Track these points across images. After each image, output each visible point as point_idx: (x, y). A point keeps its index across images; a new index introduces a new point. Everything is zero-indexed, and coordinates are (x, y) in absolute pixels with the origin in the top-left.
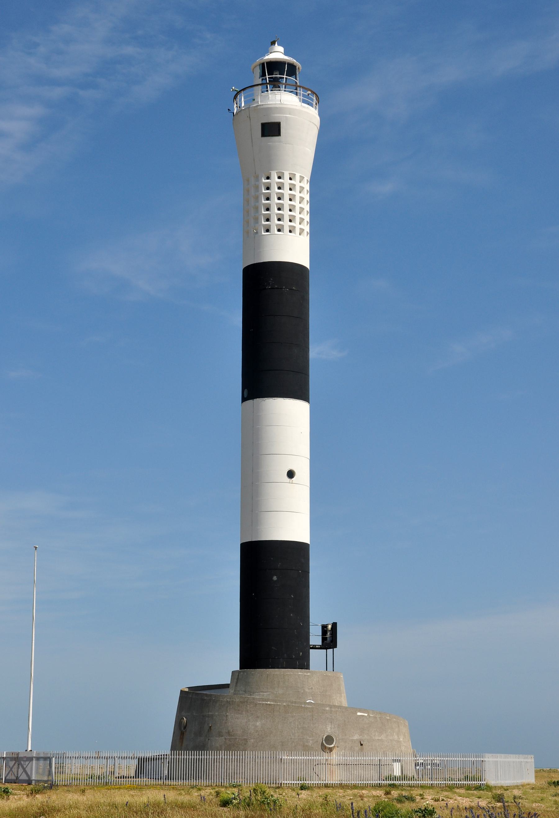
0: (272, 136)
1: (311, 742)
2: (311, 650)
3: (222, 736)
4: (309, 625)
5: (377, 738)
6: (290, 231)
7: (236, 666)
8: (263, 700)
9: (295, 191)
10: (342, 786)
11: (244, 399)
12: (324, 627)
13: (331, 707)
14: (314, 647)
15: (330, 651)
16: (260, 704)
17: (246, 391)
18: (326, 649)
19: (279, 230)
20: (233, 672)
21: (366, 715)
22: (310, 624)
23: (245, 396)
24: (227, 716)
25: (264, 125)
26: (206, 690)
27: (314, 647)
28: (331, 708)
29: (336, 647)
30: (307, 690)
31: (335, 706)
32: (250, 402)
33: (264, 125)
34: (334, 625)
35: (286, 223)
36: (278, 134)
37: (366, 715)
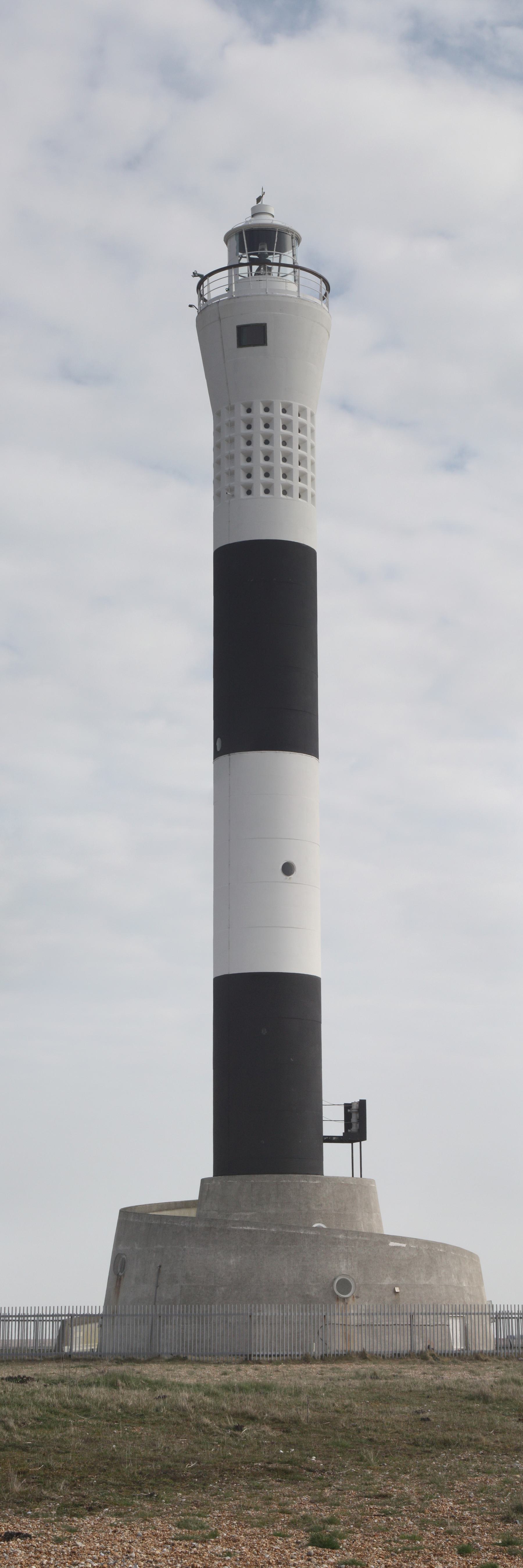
0: (254, 345)
1: (315, 1289)
2: (326, 1146)
3: (177, 1282)
4: (321, 1105)
5: (422, 1282)
6: (285, 493)
7: (208, 1172)
8: (243, 1223)
9: (291, 430)
10: (397, 1357)
11: (217, 754)
12: (347, 1107)
13: (346, 1233)
14: (330, 1139)
15: (356, 1145)
16: (236, 1230)
17: (219, 740)
18: (352, 1141)
19: (267, 491)
20: (203, 1181)
21: (404, 1245)
22: (324, 1103)
23: (218, 749)
24: (184, 1250)
25: (240, 329)
26: (173, 1209)
27: (330, 1139)
28: (346, 1235)
29: (365, 1139)
30: (314, 1208)
31: (359, 1233)
32: (224, 758)
33: (240, 329)
34: (362, 1104)
35: (279, 481)
36: (264, 342)
37: (404, 1245)
